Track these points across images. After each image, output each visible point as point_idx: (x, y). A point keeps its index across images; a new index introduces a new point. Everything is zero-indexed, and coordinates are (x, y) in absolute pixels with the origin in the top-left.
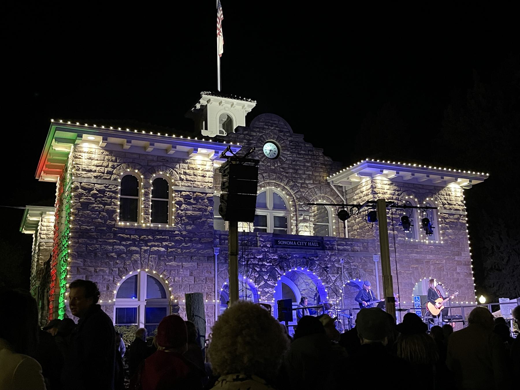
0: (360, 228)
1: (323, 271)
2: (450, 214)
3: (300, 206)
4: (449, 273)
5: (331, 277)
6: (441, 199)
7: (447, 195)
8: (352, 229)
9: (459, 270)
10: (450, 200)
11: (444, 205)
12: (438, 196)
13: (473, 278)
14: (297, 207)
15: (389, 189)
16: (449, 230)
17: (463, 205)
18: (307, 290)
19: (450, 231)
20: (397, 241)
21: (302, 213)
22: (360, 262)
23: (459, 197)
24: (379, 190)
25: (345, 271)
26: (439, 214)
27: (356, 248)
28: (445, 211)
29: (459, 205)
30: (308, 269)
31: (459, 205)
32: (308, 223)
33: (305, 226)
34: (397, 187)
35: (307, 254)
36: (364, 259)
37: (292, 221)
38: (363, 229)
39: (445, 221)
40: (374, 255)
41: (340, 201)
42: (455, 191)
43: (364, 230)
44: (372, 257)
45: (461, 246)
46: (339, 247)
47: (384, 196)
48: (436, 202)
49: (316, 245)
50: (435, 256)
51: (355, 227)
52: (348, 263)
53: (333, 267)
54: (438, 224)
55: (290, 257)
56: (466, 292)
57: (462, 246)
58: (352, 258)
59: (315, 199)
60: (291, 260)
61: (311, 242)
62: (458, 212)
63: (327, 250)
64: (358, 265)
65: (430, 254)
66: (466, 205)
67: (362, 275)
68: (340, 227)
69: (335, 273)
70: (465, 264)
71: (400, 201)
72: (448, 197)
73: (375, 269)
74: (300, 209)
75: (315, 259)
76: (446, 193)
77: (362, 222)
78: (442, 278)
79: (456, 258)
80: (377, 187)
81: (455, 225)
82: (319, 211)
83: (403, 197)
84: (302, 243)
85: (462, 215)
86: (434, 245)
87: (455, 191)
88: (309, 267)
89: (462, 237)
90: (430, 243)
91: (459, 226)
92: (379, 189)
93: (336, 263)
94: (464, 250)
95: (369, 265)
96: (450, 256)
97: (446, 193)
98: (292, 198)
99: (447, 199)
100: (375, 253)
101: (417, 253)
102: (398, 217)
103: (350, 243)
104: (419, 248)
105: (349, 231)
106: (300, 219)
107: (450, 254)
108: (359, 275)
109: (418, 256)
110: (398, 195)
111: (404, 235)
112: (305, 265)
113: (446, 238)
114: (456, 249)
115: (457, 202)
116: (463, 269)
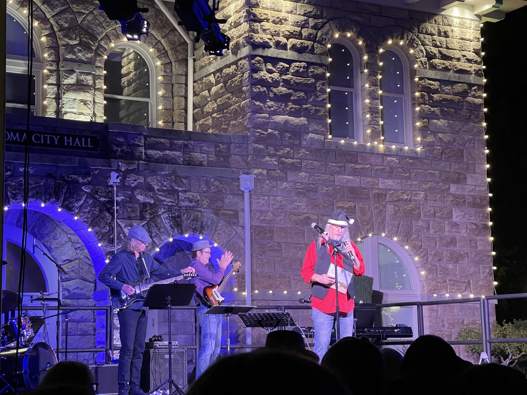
0: (221, 109)
1: (101, 211)
2: (443, 82)
3: (70, 49)
4: (431, 223)
5: (123, 226)
6: (424, 44)
7: (439, 35)
8: (203, 112)
9: (459, 218)
10: (448, 48)
11: (432, 58)
12: (418, 37)
13: (492, 239)
14: (62, 50)
15: (291, 12)
16: (438, 119)
17: (479, 60)
18: (77, 261)
19: (441, 123)
20: (304, 143)
21: (75, 66)
22: (204, 192)
23: (469, 40)
24: (266, 12)
25: (163, 213)
26: (417, 79)
27: (197, 156)
28: (431, 74)
29: (469, 61)
30: (61, 207)
31: (469, 61)
32: (88, 94)
33: (82, 101)
34: (313, 7)
35: (57, 167)
36: (217, 183)
37: (45, 86)
38: (225, 111)
39: (431, 98)
40: (244, 173)
41: (178, 44)
42: (462, 25)
43: (227, 112)
44: (239, 179)
45: (465, 160)
46: (151, 152)
47: (277, 29)
48: (412, 51)
49: (86, 143)
50: (399, 181)
51: (210, 107)
52: (172, 192)
53: (130, 202)
54: (414, 105)
55: (9, 173)
56: (472, 269)
57: (469, 160)
58: (184, 180)
59: (113, 34)
60: (12, 181)
61: (71, 136)
62: (464, 78)
63: (116, 158)
64: (199, 198)
65: (390, 177)
66: (485, 60)
67: (209, 223)
68: (175, 107)
69: (135, 218)
70: (474, 204)
71: (320, 42)
72: (443, 39)
73: (243, 210)
74: (69, 56)
75: (81, 180)
76: (439, 30)
77: (223, 94)
78: (414, 236)
79: (453, 188)
80: (261, 5)
81: (454, 109)
82: (138, 71)
83: (327, 34)
84: (45, 139)
85: (474, 85)
86: (400, 155)
87: (462, 25)
88: (64, 202)
89: (471, 137)
90: (388, 149)
91: (464, 112)
92: (267, 9)
93: (138, 191)
94: (474, 169)
95: (229, 199)
96: (438, 183)
97: (439, 30)
98: (49, 26)
99: (438, 44)
100: (246, 171)
101: (355, 172)
102: (312, 83)
103: (181, 142)
104: (359, 161)
105: (196, 117)
106: (67, 81)
107: (438, 179)
108: (199, 223)
109: (355, 181)
110: (315, 27)
111: (323, 127)
112: (50, 194)
113: (430, 139)
114: (455, 167)
115: (464, 53)
116: (467, 216)
